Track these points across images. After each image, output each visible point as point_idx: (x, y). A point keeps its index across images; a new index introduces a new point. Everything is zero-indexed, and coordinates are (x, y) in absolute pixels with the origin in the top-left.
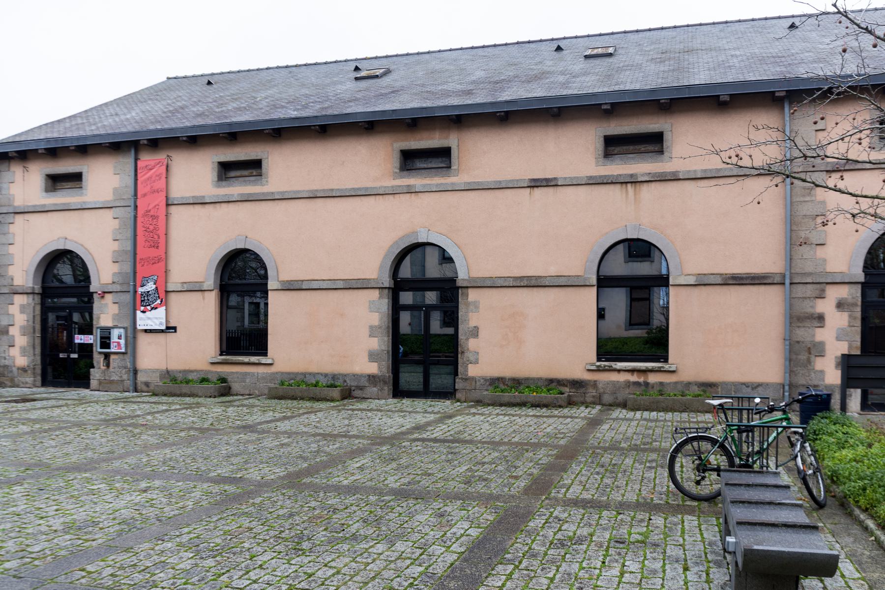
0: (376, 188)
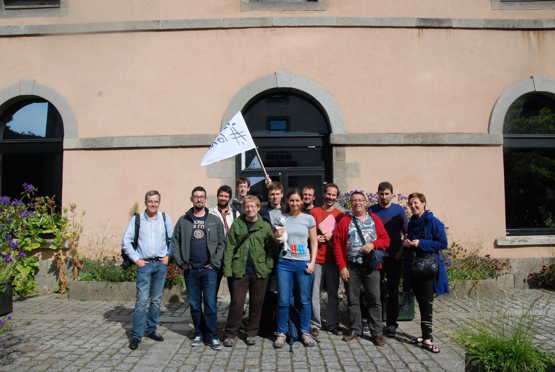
0: (219, 20)
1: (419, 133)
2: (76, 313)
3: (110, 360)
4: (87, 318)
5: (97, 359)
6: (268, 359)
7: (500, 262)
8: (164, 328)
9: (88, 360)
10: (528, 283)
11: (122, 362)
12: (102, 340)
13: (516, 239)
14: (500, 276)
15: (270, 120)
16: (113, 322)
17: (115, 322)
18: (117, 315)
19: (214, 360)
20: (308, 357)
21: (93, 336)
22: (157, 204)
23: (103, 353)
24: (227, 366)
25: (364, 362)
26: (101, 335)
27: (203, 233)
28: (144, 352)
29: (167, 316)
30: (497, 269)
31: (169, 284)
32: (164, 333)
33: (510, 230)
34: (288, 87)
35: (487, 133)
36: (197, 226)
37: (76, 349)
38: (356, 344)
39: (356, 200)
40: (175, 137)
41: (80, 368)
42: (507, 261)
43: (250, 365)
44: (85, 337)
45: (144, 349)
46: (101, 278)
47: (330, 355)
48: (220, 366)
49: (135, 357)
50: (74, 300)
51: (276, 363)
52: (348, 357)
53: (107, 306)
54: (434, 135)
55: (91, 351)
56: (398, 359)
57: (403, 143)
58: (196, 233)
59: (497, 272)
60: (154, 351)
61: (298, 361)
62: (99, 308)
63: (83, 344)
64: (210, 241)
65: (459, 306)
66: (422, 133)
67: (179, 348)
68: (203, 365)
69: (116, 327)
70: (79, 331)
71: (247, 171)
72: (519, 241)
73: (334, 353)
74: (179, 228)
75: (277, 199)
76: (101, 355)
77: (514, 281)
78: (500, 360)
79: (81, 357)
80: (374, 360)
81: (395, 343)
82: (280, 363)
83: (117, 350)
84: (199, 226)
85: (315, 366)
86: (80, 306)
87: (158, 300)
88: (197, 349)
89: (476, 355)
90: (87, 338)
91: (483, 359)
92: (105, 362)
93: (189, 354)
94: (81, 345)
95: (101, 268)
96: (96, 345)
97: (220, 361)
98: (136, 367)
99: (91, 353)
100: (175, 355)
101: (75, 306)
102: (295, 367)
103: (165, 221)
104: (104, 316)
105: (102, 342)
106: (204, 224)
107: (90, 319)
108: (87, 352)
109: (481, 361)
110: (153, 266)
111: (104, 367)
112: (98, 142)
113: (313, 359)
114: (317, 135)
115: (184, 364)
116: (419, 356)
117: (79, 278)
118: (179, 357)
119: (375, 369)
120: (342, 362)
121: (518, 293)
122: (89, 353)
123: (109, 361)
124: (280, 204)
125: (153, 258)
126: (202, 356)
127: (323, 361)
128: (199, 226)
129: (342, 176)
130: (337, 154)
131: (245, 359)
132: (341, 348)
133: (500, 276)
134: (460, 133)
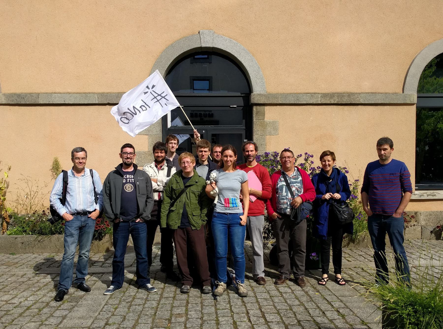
1: (336, 93)
2: (5, 267)
3: (38, 315)
4: (17, 272)
5: (25, 315)
6: (194, 307)
7: (408, 214)
8: (95, 278)
9: (16, 316)
10: (435, 235)
11: (52, 315)
12: (31, 294)
13: (424, 193)
14: (408, 227)
15: (194, 80)
16: (43, 275)
17: (45, 275)
18: (47, 268)
19: (142, 310)
20: (231, 304)
21: (22, 290)
22: (84, 161)
23: (32, 307)
24: (155, 316)
25: (283, 309)
26: (31, 289)
27: (133, 187)
28: (74, 304)
29: (97, 266)
30: (406, 221)
31: (98, 236)
32: (95, 284)
33: (419, 185)
34: (212, 46)
35: (402, 92)
36: (126, 181)
37: (4, 305)
38: (275, 291)
39: (285, 157)
40: (102, 94)
41: (7, 324)
42: (415, 214)
43: (177, 314)
44: (13, 292)
45: (74, 301)
46: (32, 232)
47: (251, 303)
48: (148, 315)
49: (65, 310)
50: (3, 254)
51: (201, 311)
52: (269, 304)
53: (37, 259)
54: (350, 95)
55: (19, 306)
56: (315, 306)
57: (320, 102)
58: (126, 187)
59: (406, 224)
60: (84, 302)
61: (222, 309)
62: (30, 261)
63: (11, 299)
64: (139, 194)
65: (370, 255)
66: (338, 93)
67: (109, 299)
68: (132, 315)
69: (47, 279)
70: (7, 286)
71: (173, 129)
72: (428, 195)
73: (255, 301)
74: (109, 183)
75: (205, 156)
76: (30, 310)
77: (422, 233)
78: (419, 314)
79: (8, 313)
80: (293, 308)
81: (312, 291)
82: (205, 311)
83: (46, 303)
84: (128, 180)
85: (238, 313)
86: (9, 260)
87: (86, 253)
88: (126, 299)
89: (395, 309)
90: (15, 293)
91: (402, 313)
92: (34, 316)
93: (118, 304)
94: (9, 300)
95: (31, 221)
96: (25, 299)
97: (148, 311)
98: (65, 321)
99: (19, 308)
100: (104, 306)
101: (4, 260)
102: (219, 315)
103: (92, 177)
104: (34, 269)
105: (31, 296)
106: (133, 178)
107: (19, 273)
108: (15, 307)
109: (399, 315)
110: (81, 220)
111: (32, 322)
112: (23, 98)
113: (236, 306)
114: (239, 94)
115: (113, 315)
116: (335, 304)
117: (8, 232)
118: (109, 308)
119: (294, 316)
120: (263, 310)
121: (426, 244)
122: (17, 308)
123: (38, 316)
124: (207, 160)
125: (81, 213)
126: (130, 306)
127: (245, 309)
128: (128, 180)
129: (261, 134)
130: (257, 114)
131: (172, 308)
132: (261, 296)
133: (408, 227)
134: (375, 93)
